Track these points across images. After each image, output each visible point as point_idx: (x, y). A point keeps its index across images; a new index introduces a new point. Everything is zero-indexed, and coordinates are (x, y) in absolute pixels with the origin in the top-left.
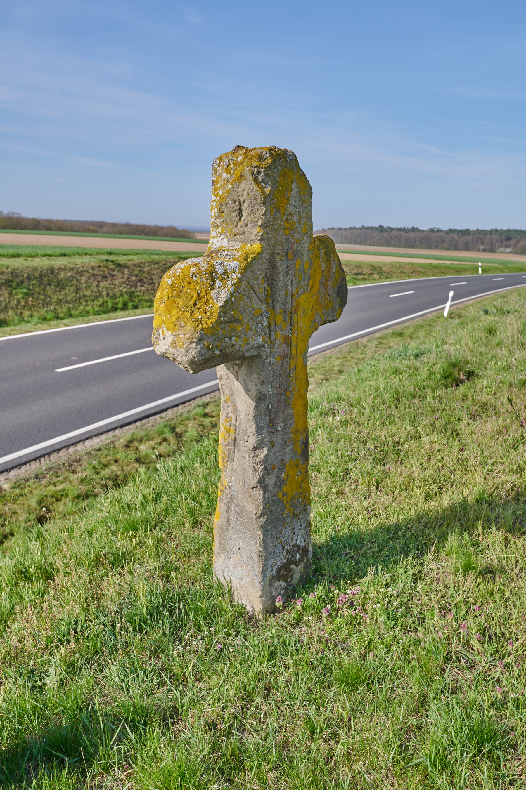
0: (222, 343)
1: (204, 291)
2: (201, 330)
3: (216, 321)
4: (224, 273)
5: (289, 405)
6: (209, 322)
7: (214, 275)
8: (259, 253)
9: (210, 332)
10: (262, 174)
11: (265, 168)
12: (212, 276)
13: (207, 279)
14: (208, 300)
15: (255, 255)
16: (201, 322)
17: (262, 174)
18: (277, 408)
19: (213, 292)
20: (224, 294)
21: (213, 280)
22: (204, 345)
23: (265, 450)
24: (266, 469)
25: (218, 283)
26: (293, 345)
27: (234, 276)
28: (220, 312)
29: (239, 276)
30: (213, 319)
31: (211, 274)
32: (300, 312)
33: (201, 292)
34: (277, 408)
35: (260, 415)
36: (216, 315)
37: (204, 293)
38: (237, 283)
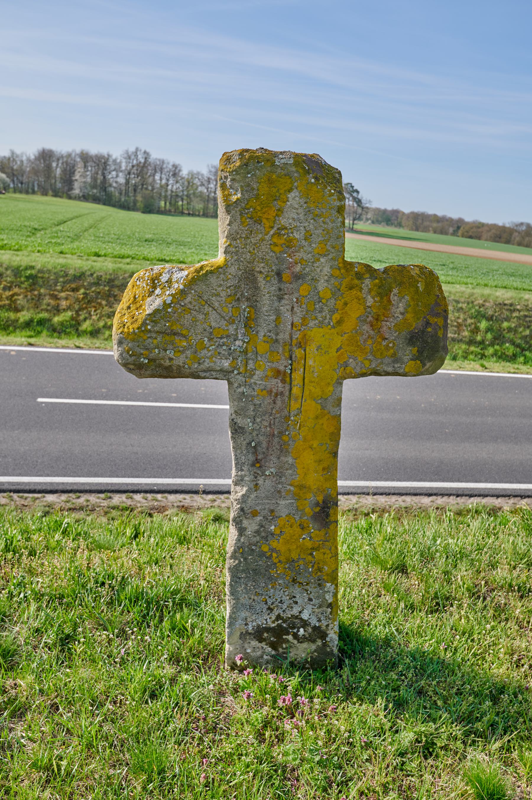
0: (151, 352)
1: (141, 296)
2: (121, 333)
3: (138, 328)
4: (166, 282)
5: (287, 451)
6: (131, 327)
7: (156, 282)
8: (219, 267)
9: (130, 337)
10: (229, 180)
11: (229, 172)
12: (153, 282)
13: (147, 285)
14: (141, 306)
15: (213, 269)
16: (124, 325)
17: (229, 180)
18: (268, 449)
19: (149, 299)
20: (158, 303)
21: (155, 287)
22: (125, 349)
23: (245, 489)
24: (242, 509)
25: (158, 291)
26: (294, 383)
27: (176, 286)
28: (146, 319)
29: (181, 287)
30: (136, 326)
31: (153, 280)
32: (311, 349)
33: (139, 296)
34: (268, 449)
35: (241, 448)
36: (140, 322)
37: (141, 298)
38: (176, 294)
